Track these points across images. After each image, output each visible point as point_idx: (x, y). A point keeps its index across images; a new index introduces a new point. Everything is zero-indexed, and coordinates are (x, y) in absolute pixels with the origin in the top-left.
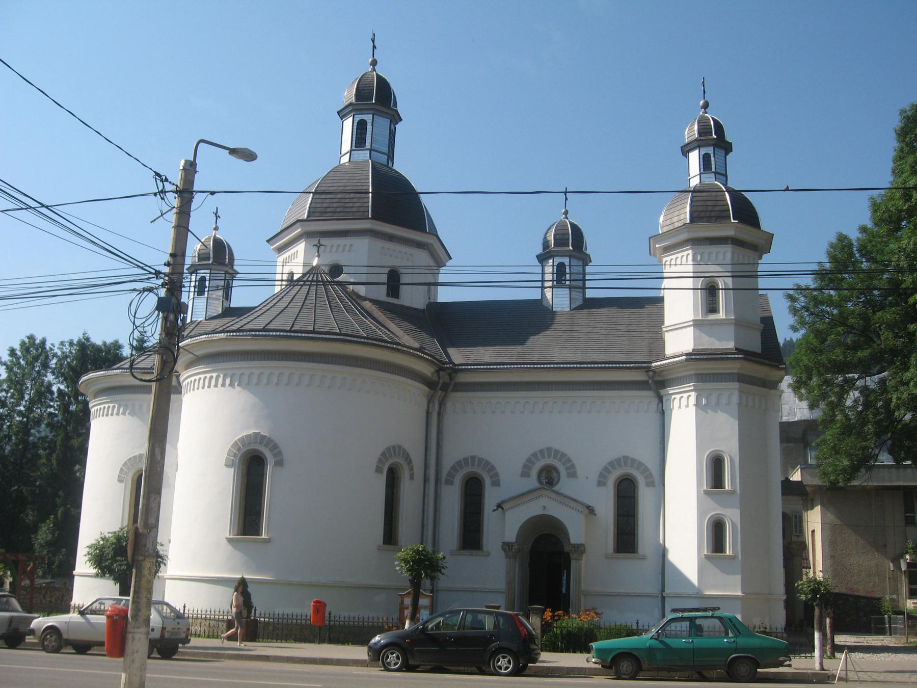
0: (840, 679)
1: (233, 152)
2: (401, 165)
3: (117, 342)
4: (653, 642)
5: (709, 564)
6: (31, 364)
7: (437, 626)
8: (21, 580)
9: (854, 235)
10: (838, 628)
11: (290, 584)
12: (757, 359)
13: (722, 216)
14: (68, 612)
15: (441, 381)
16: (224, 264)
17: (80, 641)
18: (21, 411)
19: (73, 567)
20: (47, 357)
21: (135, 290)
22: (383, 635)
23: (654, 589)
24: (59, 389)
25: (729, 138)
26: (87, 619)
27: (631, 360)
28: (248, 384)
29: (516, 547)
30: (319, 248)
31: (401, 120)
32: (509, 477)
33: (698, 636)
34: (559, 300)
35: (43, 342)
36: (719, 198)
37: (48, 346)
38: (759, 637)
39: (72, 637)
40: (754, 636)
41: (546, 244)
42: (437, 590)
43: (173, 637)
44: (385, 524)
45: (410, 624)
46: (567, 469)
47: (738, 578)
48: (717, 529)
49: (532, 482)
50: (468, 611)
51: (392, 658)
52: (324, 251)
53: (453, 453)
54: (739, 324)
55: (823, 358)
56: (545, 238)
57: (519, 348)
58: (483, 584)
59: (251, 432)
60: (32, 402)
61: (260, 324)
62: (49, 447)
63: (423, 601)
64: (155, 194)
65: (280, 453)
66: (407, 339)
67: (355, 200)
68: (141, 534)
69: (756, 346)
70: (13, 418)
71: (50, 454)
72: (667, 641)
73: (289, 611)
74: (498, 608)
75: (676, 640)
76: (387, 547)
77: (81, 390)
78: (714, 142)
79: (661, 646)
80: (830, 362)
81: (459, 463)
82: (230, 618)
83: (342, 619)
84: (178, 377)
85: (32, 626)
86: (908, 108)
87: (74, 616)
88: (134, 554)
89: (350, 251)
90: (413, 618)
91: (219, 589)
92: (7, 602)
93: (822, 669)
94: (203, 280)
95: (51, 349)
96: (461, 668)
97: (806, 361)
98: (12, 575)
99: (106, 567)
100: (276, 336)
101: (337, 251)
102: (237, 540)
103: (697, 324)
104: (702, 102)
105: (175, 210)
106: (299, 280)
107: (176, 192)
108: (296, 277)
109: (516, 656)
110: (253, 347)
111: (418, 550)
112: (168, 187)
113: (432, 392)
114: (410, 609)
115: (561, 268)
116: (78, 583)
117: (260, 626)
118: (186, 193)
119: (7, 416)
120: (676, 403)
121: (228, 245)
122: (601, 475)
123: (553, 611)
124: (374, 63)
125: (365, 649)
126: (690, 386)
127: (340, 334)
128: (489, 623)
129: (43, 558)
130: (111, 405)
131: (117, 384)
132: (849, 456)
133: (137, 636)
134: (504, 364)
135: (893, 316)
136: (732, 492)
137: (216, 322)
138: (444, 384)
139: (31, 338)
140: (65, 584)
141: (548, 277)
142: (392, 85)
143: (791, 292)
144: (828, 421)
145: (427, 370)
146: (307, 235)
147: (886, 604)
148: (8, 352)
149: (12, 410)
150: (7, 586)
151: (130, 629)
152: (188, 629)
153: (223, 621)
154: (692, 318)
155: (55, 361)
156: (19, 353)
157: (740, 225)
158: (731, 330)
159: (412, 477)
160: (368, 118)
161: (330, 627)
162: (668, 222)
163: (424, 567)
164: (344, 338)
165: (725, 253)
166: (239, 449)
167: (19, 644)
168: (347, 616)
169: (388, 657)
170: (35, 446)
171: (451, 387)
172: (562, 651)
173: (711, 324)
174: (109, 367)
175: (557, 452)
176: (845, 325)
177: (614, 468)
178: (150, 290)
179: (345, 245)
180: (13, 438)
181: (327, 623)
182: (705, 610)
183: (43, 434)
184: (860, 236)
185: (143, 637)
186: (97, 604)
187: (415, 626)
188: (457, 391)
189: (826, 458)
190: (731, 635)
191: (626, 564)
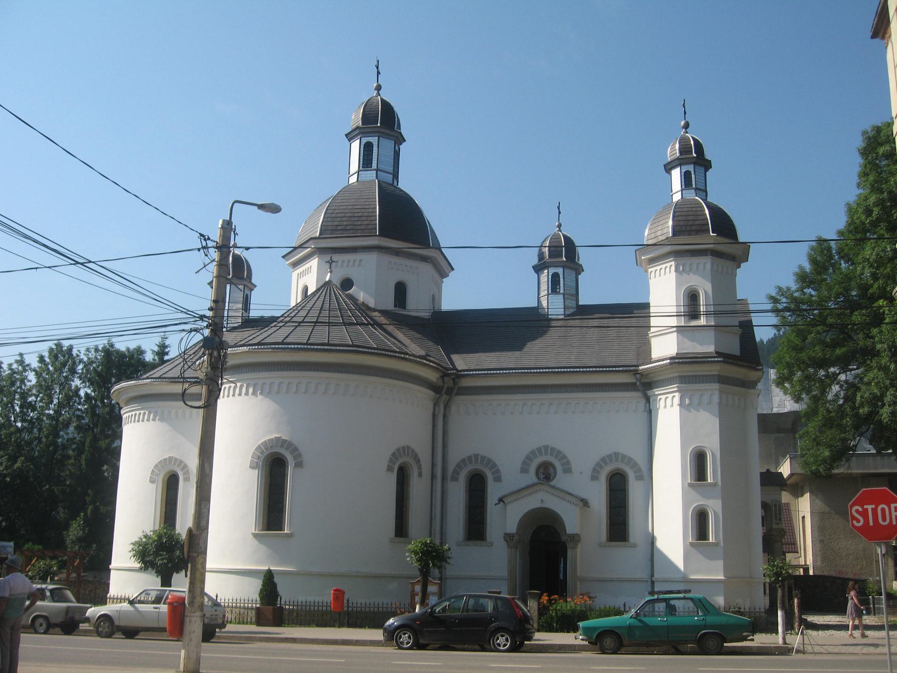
0: (798, 651)
1: (261, 207)
2: (406, 184)
3: (139, 347)
4: (632, 620)
5: (694, 551)
6: (59, 370)
7: (444, 609)
11: (311, 574)
13: (702, 229)
15: (446, 386)
16: (242, 278)
18: (49, 415)
20: (74, 363)
21: (183, 330)
22: (396, 618)
23: (644, 574)
24: (86, 394)
25: (708, 156)
28: (269, 393)
29: (516, 537)
32: (510, 474)
33: (672, 615)
34: (554, 306)
36: (699, 213)
37: (75, 352)
39: (123, 623)
41: (541, 256)
42: (445, 579)
45: (420, 608)
46: (563, 465)
47: (721, 563)
48: (700, 520)
49: (531, 478)
50: (470, 596)
51: (405, 638)
53: (458, 451)
55: (803, 356)
57: (517, 354)
58: (486, 571)
59: (273, 436)
60: (60, 405)
63: (432, 588)
64: (199, 250)
65: (300, 455)
66: (415, 349)
72: (644, 619)
74: (500, 593)
75: (655, 619)
76: (398, 539)
79: (640, 624)
80: (809, 358)
81: (463, 460)
82: (258, 605)
83: (359, 605)
85: (87, 615)
86: (869, 130)
88: (189, 552)
89: (359, 266)
90: (423, 603)
91: (246, 580)
93: (785, 643)
95: (78, 356)
96: (466, 646)
97: (788, 359)
99: (148, 561)
101: (348, 266)
102: (262, 535)
103: (680, 329)
104: (683, 123)
105: (215, 263)
106: (314, 294)
107: (217, 248)
109: (513, 634)
111: (426, 543)
112: (210, 244)
113: (438, 396)
114: (420, 595)
115: (555, 277)
117: (286, 613)
120: (662, 403)
121: (246, 261)
123: (549, 596)
124: (378, 88)
125: (381, 631)
126: (674, 387)
127: (353, 346)
128: (490, 607)
130: (142, 412)
131: (148, 392)
133: (193, 619)
136: (714, 485)
138: (448, 388)
141: (544, 287)
142: (396, 109)
144: (811, 413)
145: (432, 376)
146: (320, 251)
147: (871, 585)
151: (187, 613)
152: (224, 616)
153: (252, 608)
155: (81, 366)
159: (420, 475)
160: (374, 140)
161: (348, 613)
163: (432, 558)
166: (262, 452)
167: (73, 631)
168: (363, 602)
169: (401, 637)
171: (455, 391)
175: (553, 449)
176: (824, 324)
177: (606, 464)
178: (196, 330)
181: (346, 609)
182: (679, 592)
183: (71, 436)
186: (143, 595)
187: (424, 610)
190: (700, 614)
191: (618, 551)
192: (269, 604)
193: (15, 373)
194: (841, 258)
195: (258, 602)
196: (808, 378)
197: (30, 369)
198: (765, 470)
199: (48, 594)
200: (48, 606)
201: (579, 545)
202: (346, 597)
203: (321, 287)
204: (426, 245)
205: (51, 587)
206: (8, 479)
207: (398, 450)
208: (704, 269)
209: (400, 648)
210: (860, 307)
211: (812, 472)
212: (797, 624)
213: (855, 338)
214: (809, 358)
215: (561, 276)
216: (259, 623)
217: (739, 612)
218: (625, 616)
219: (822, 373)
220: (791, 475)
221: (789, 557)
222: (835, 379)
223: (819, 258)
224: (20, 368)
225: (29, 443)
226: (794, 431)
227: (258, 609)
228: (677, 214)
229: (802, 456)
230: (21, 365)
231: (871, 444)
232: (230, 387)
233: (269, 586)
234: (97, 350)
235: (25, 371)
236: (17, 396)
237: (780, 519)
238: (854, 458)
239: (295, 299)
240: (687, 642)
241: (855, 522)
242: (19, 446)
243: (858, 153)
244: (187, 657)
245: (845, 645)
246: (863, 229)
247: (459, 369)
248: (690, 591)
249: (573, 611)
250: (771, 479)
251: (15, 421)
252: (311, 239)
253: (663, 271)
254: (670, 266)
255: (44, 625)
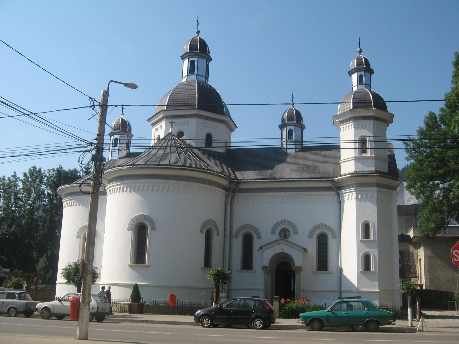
0: (419, 331)
1: (126, 85)
2: (212, 82)
3: (76, 169)
4: (329, 313)
6: (34, 181)
8: (31, 285)
9: (437, 113)
10: (423, 307)
11: (159, 287)
12: (387, 176)
14: (54, 300)
15: (232, 188)
16: (126, 132)
17: (60, 314)
18: (29, 204)
19: (56, 279)
20: (42, 177)
21: (81, 151)
22: (201, 310)
23: (336, 288)
24: (48, 193)
25: (372, 67)
26: (62, 304)
27: (325, 177)
29: (269, 268)
30: (172, 123)
31: (212, 60)
32: (266, 234)
35: (40, 170)
36: (367, 97)
38: (380, 311)
40: (377, 310)
41: (283, 120)
43: (103, 312)
44: (205, 258)
45: (215, 305)
46: (293, 230)
47: (377, 283)
48: (366, 260)
49: (277, 236)
50: (241, 299)
51: (206, 321)
52: (175, 125)
54: (377, 158)
55: (421, 174)
56: (283, 117)
57: (270, 171)
58: (253, 286)
59: (140, 213)
60: (35, 199)
61: (143, 161)
62: (43, 221)
63: (222, 295)
64: (90, 107)
65: (154, 224)
66: (216, 168)
67: (189, 100)
68: (86, 264)
69: (385, 169)
70: (26, 207)
71: (44, 224)
72: (335, 312)
73: (158, 299)
74: (258, 297)
75: (341, 312)
77: (58, 194)
78: (364, 69)
80: (425, 175)
81: (241, 227)
82: (130, 303)
83: (184, 303)
84: (105, 187)
87: (56, 302)
88: (82, 273)
89: (187, 125)
90: (216, 303)
92: (25, 295)
93: (412, 326)
94: (116, 139)
95: (44, 173)
96: (239, 326)
98: (27, 283)
100: (151, 167)
101: (181, 125)
102: (134, 266)
103: (356, 159)
104: (358, 50)
105: (99, 114)
107: (100, 106)
108: (161, 138)
109: (264, 320)
110: (141, 172)
112: (96, 103)
115: (290, 131)
116: (58, 286)
118: (104, 106)
119: (22, 206)
120: (346, 197)
121: (129, 123)
122: (310, 233)
123: (285, 299)
124: (198, 32)
125: (193, 317)
126: (353, 189)
128: (252, 304)
129: (41, 275)
130: (73, 201)
132: (435, 222)
133: (84, 310)
134: (264, 179)
135: (454, 153)
136: (374, 241)
137: (123, 160)
138: (233, 189)
139: (34, 168)
140: (52, 287)
141: (284, 136)
142: (207, 43)
143: (406, 141)
144: (425, 205)
145: (225, 183)
146: (166, 117)
147: (456, 295)
148: (23, 175)
149: (25, 203)
150: (25, 289)
151: (81, 307)
153: (127, 304)
154: (354, 156)
155: (45, 179)
156: (28, 175)
157: (377, 110)
158: (373, 162)
159: (218, 235)
160: (195, 59)
161: (178, 307)
162: (342, 109)
163: (222, 278)
164: (184, 168)
165: (370, 124)
166: (134, 222)
168: (186, 301)
169: (203, 321)
170: (37, 220)
172: (289, 318)
173: (363, 159)
174: (71, 183)
175: (288, 222)
176: (433, 157)
177: (316, 229)
178: (88, 151)
179: (185, 122)
180: (26, 217)
181: (177, 305)
182: (354, 298)
183: (40, 215)
184: (440, 113)
185: (87, 310)
186: (67, 296)
188: (240, 192)
189: (424, 223)
190: (366, 310)
191: (323, 276)
192: (135, 302)
193: (12, 182)
194: (442, 123)
195: (130, 301)
196: (424, 186)
197: (20, 180)
198: (400, 234)
199: (17, 295)
200: (17, 302)
201: (302, 273)
202: (177, 299)
203: (167, 136)
204: (222, 113)
205: (18, 292)
206: (7, 236)
207: (206, 221)
208: (369, 126)
209: (203, 327)
210: (451, 148)
211: (425, 235)
212: (418, 315)
213: (449, 165)
214: (425, 175)
215: (294, 131)
216: (130, 312)
217: (387, 309)
218: (325, 310)
219: (431, 183)
220: (414, 237)
221: (413, 280)
222: (438, 187)
223: (430, 123)
224: (14, 179)
225: (19, 218)
226: (415, 214)
227: (130, 304)
228: (355, 97)
229: (420, 227)
230: (15, 178)
231: (456, 221)
232: (120, 187)
233: (136, 292)
234: (54, 170)
235: (17, 181)
236: (13, 194)
237: (409, 260)
238: (447, 229)
239: (153, 142)
240: (358, 325)
241: (455, 259)
242: (13, 220)
243: (452, 65)
244: (81, 331)
245: (445, 327)
246: (455, 105)
247: (239, 179)
248: (360, 297)
249: (298, 307)
250: (404, 238)
251: (12, 207)
252: (162, 110)
253: (347, 127)
254: (351, 125)
255: (14, 312)
